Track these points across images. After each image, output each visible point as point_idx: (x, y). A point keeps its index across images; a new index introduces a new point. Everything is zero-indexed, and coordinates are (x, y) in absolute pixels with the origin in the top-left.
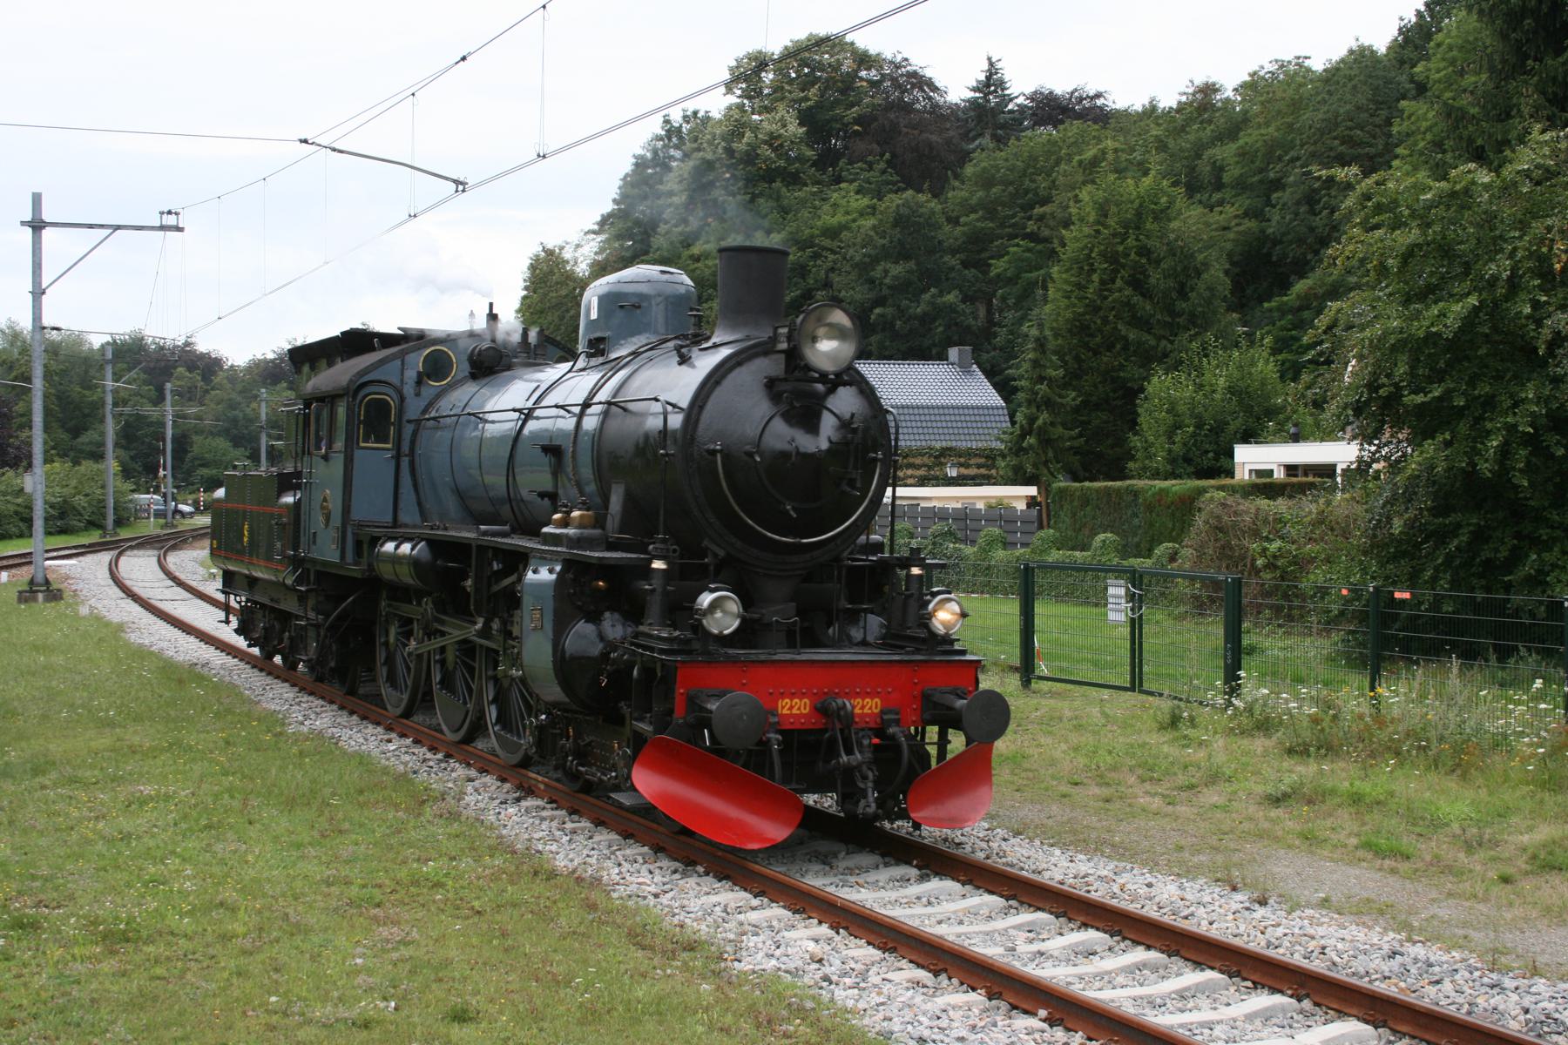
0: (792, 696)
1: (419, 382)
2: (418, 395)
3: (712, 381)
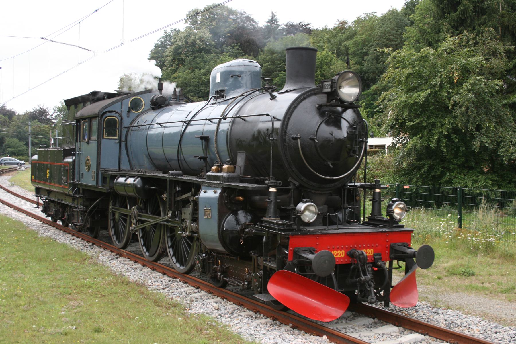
0: (337, 249)
3: (293, 106)
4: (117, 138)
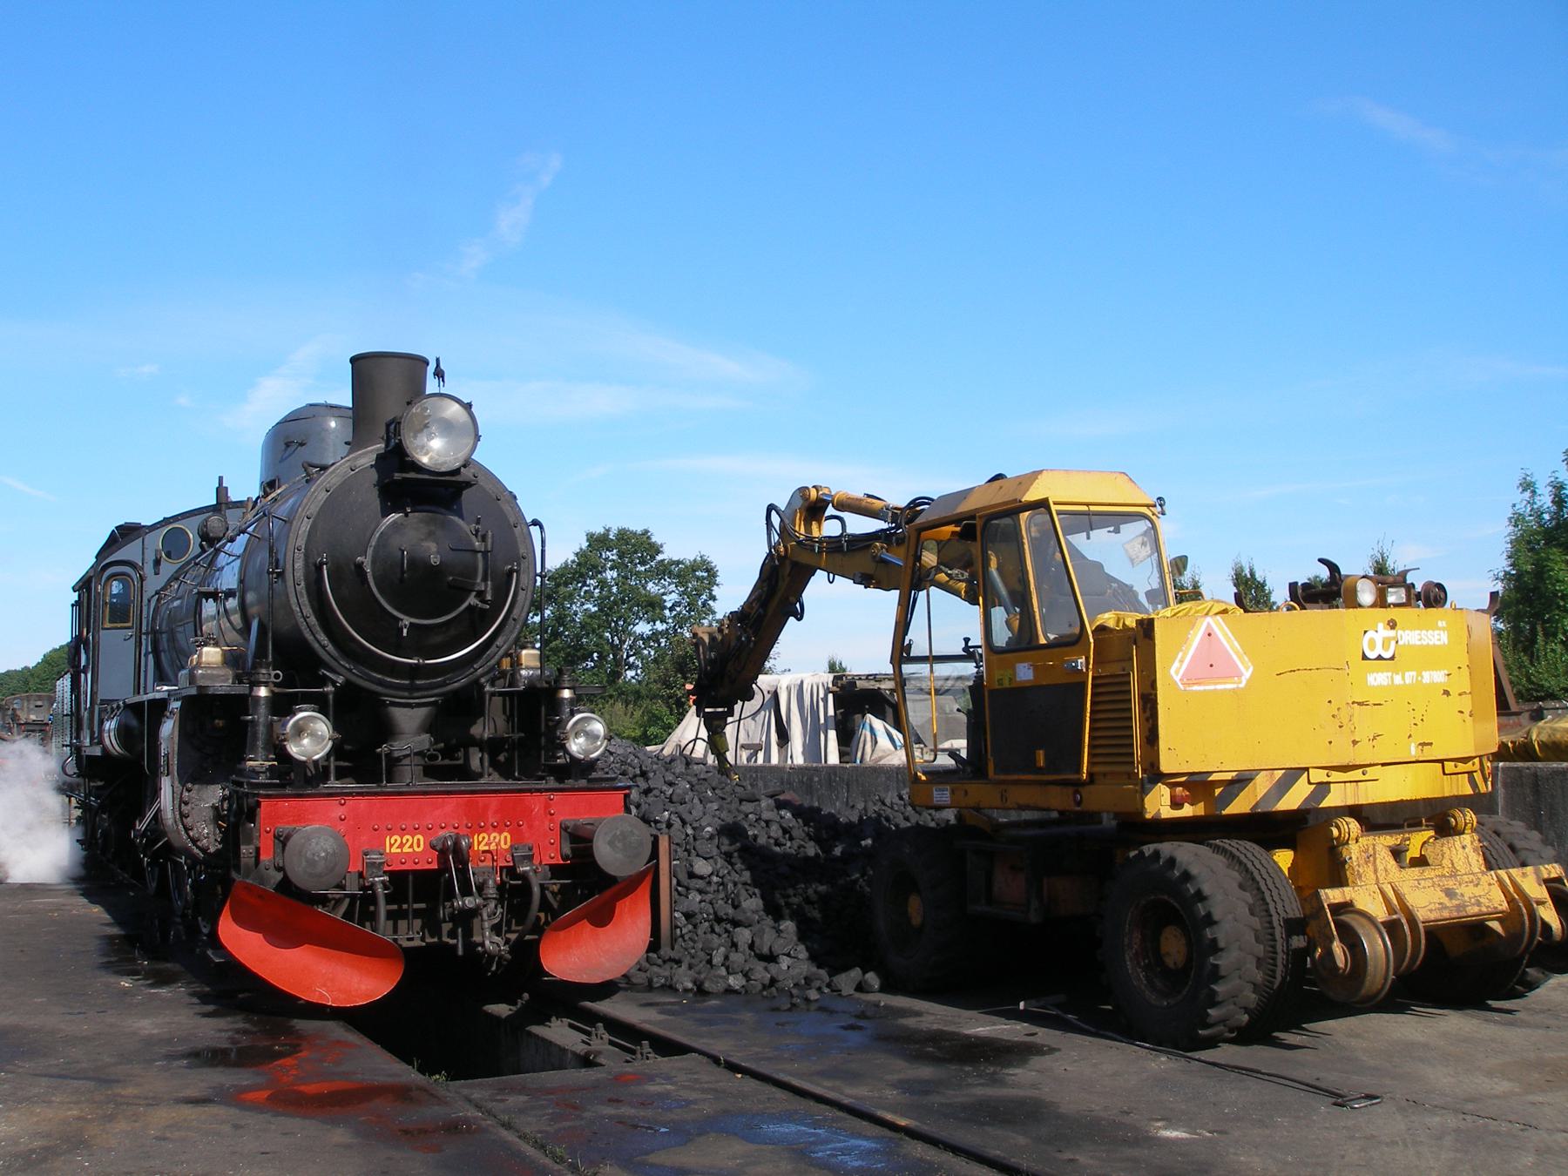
0: (403, 832)
1: (157, 562)
2: (157, 573)
4: (130, 624)
